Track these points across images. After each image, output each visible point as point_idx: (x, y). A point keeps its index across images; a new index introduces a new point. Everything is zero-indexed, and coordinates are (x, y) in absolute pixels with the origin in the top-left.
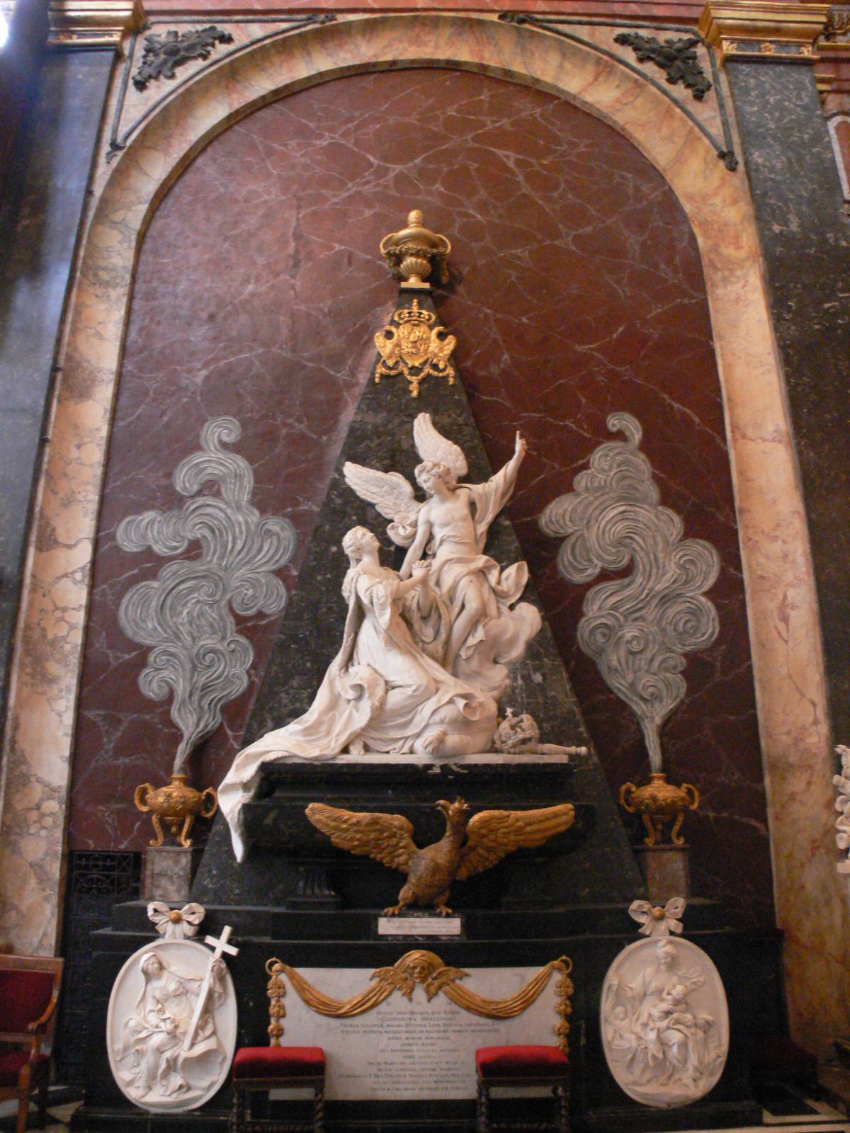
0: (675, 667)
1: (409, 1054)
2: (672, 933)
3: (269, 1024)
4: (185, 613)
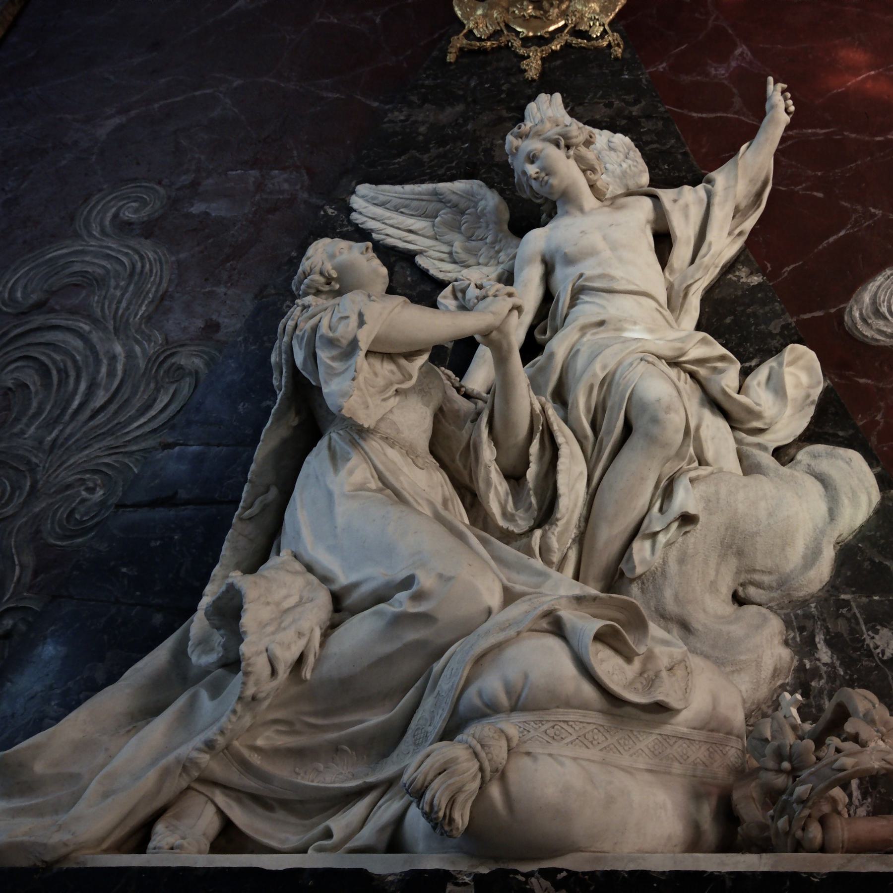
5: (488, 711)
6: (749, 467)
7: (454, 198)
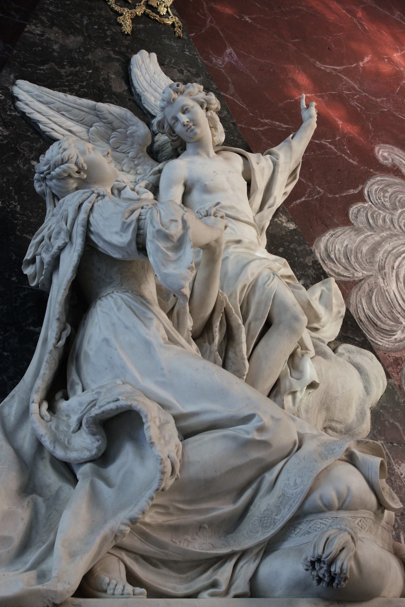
5: (325, 509)
7: (110, 117)
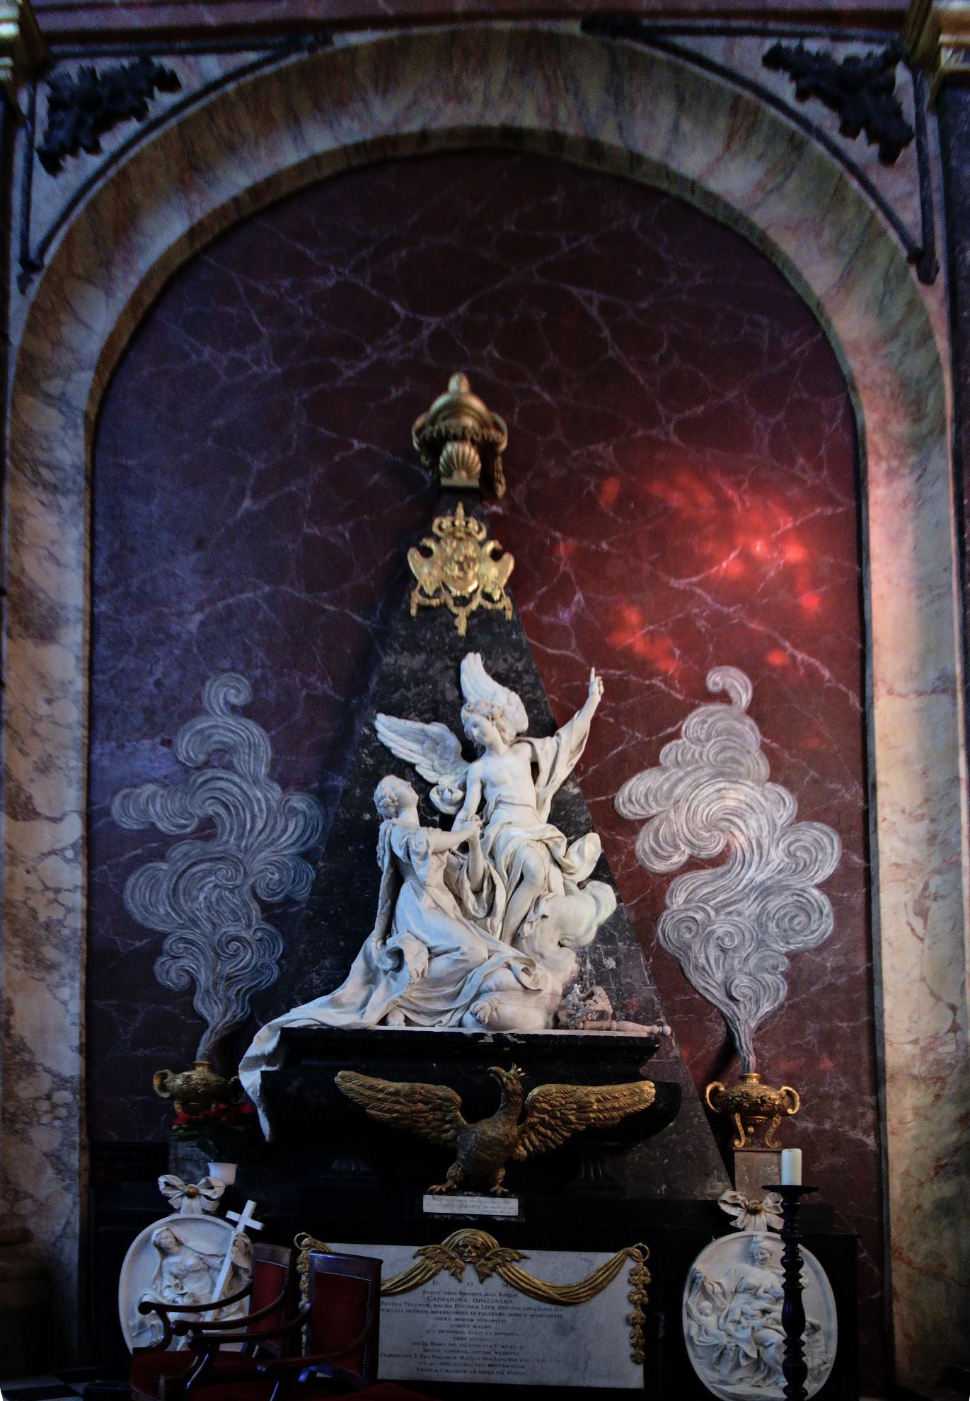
0: (775, 968)
1: (460, 1335)
2: (770, 1229)
3: (300, 1299)
4: (201, 898)
6: (568, 892)
